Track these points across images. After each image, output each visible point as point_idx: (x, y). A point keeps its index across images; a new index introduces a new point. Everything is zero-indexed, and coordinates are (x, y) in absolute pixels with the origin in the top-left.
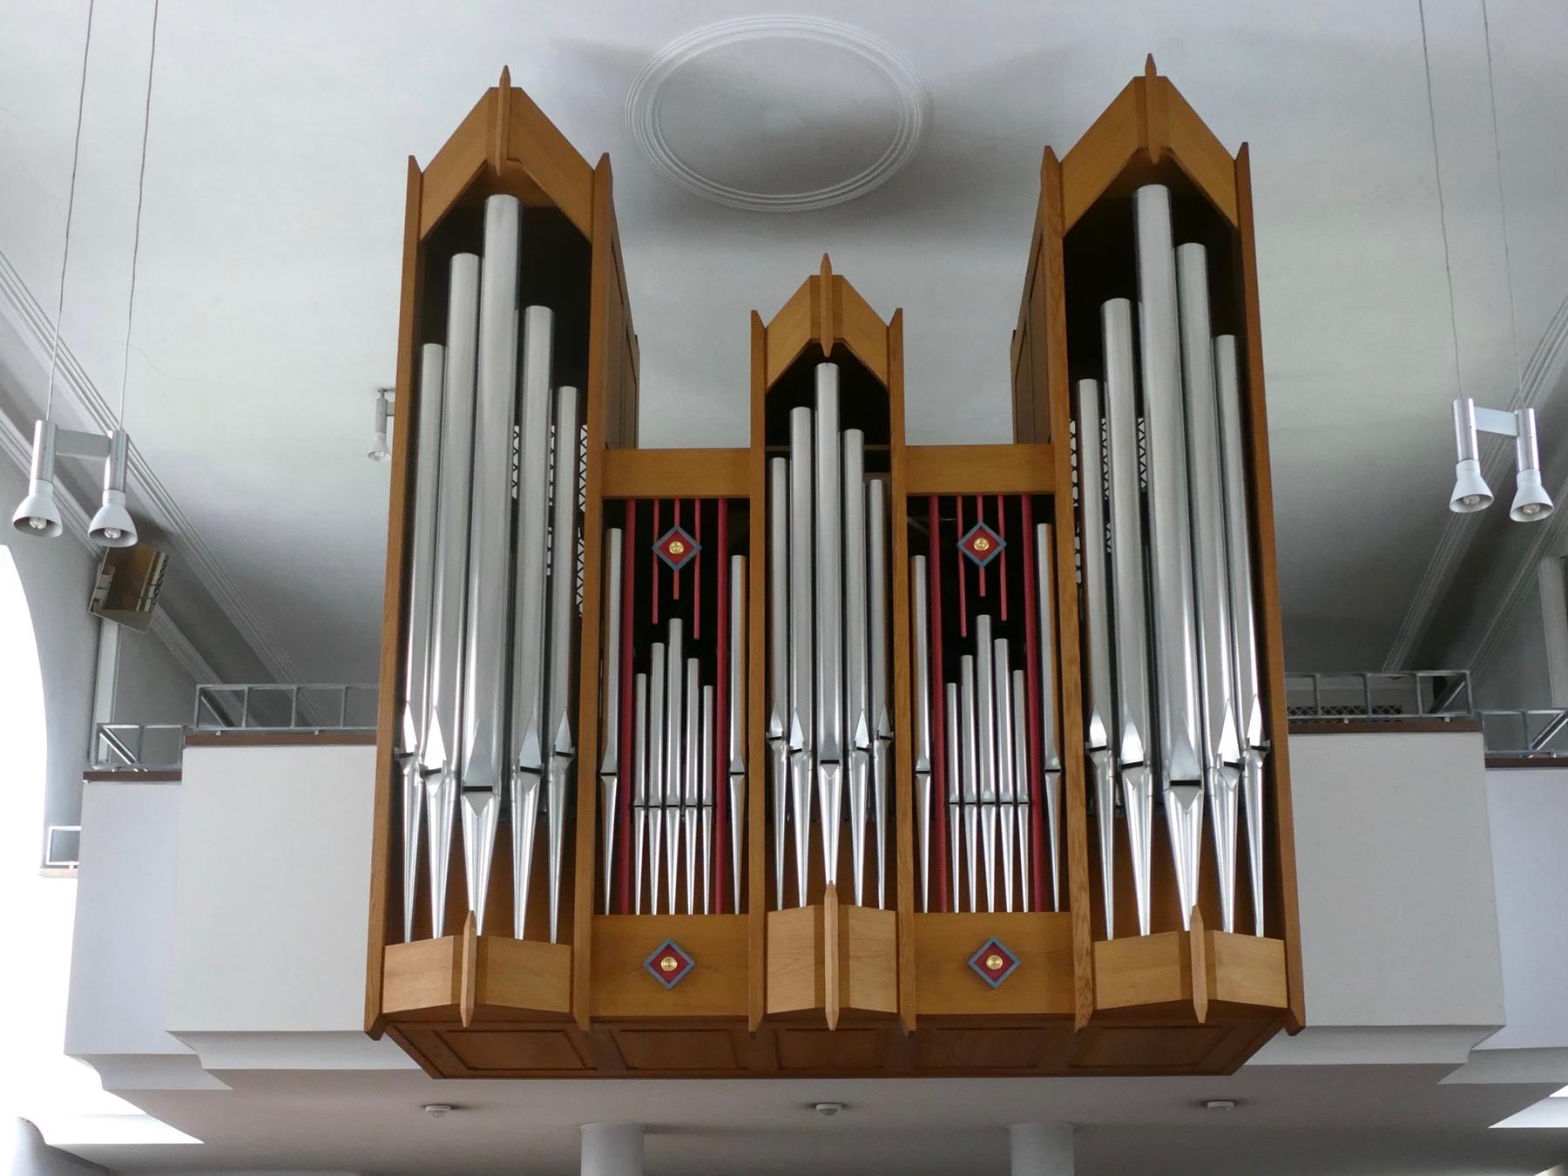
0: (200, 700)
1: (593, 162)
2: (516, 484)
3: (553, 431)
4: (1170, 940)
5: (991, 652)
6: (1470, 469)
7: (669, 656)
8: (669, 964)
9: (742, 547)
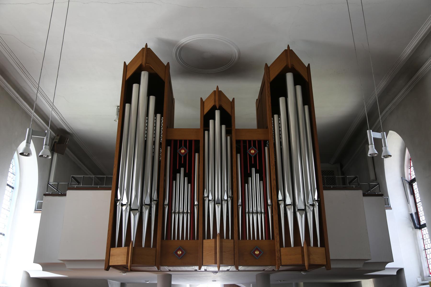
0: (72, 179)
1: (166, 64)
2: (146, 137)
3: (155, 118)
4: (299, 249)
5: (255, 177)
6: (372, 147)
7: (181, 177)
8: (180, 253)
9: (197, 151)
